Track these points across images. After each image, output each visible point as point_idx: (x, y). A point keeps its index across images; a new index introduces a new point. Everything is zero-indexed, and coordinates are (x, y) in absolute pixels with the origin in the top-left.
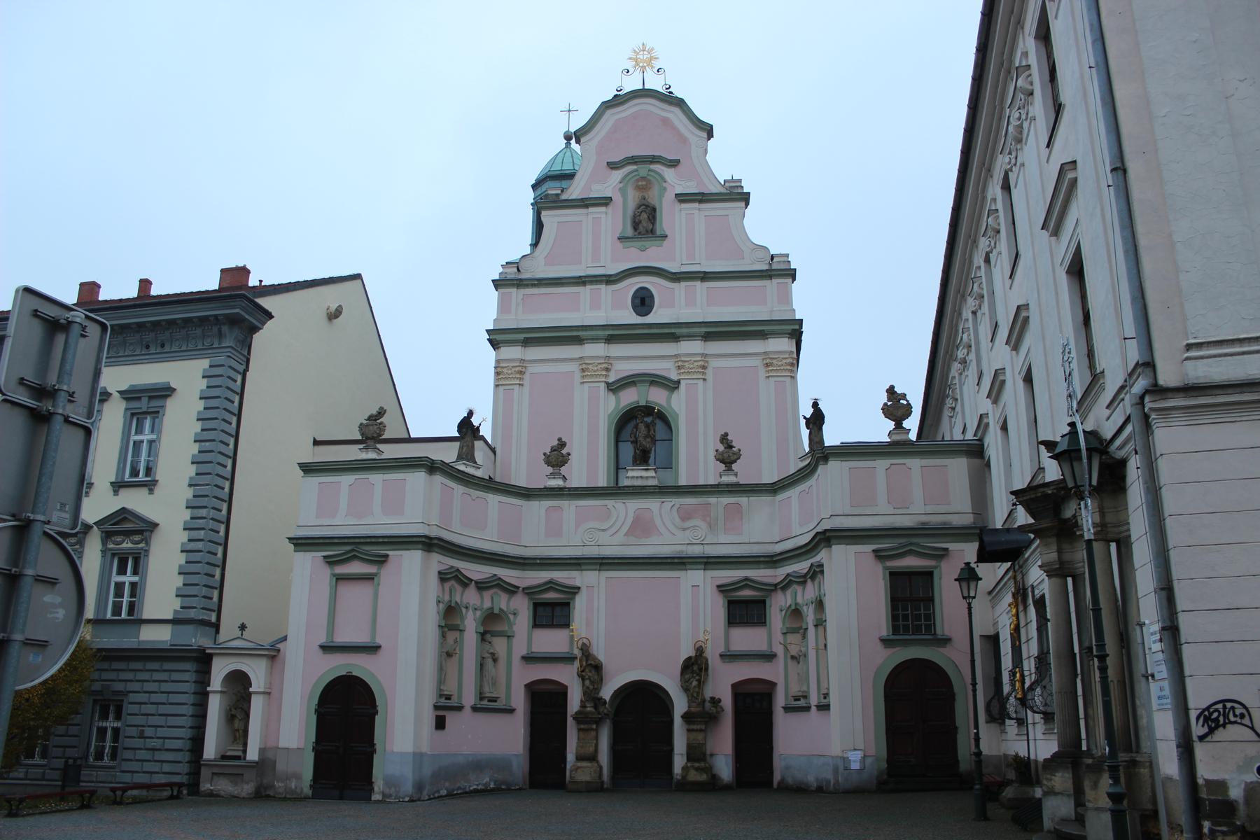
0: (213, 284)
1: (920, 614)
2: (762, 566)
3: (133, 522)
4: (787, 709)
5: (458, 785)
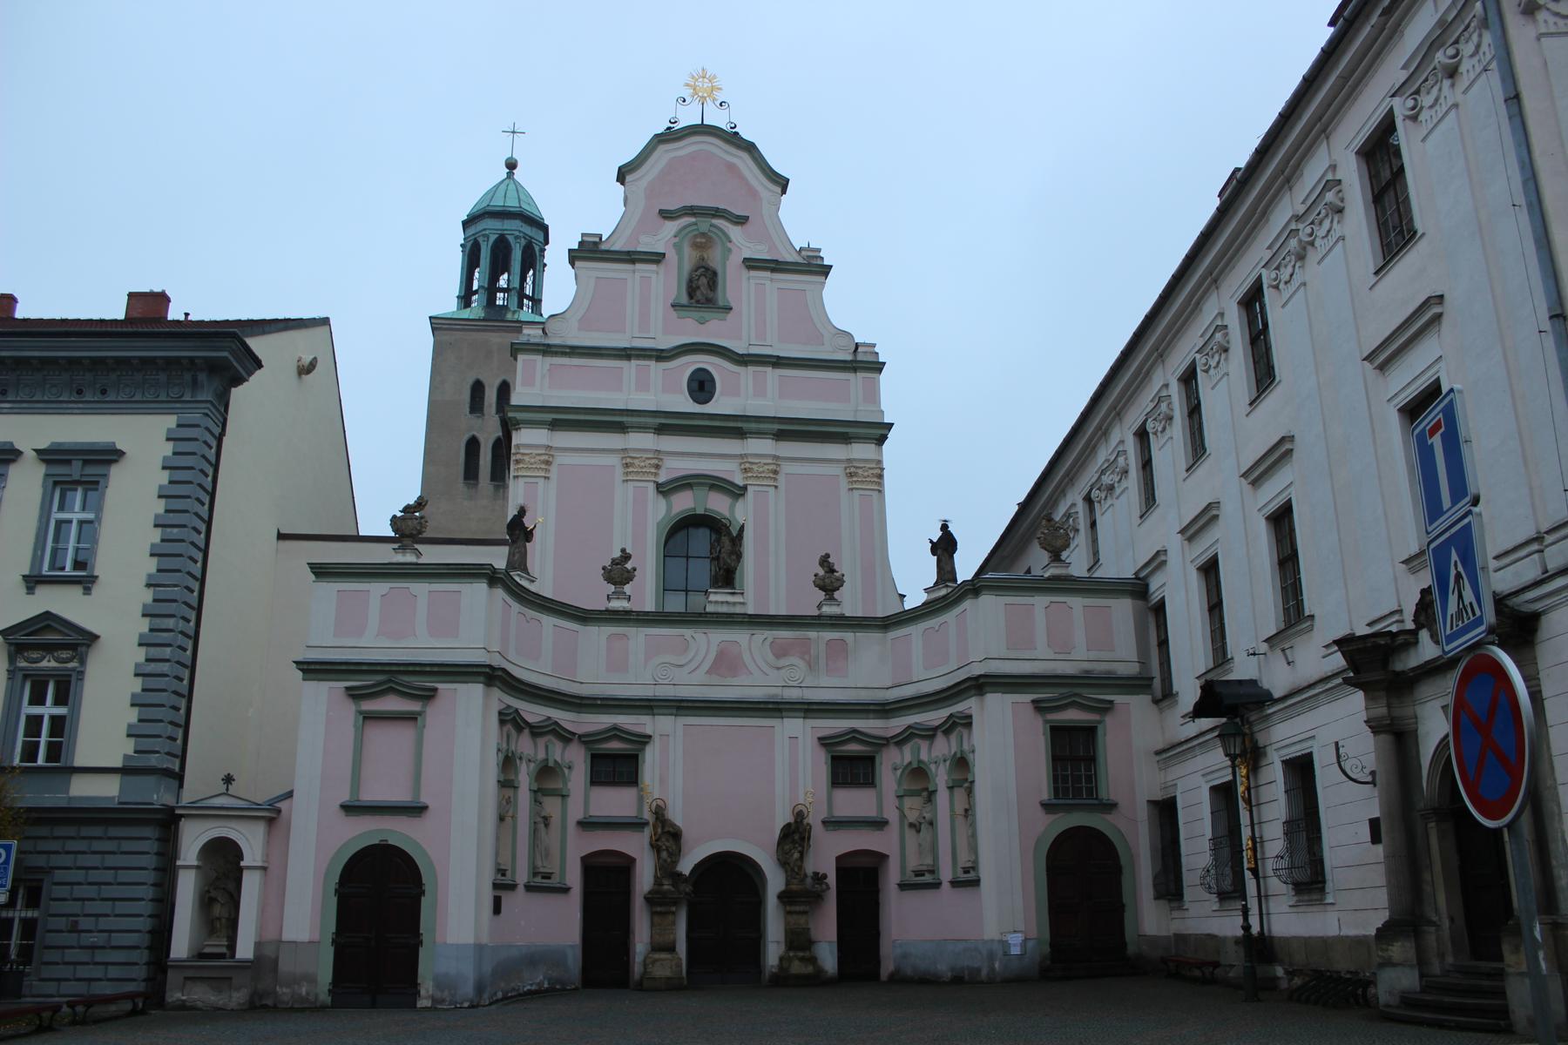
0: (116, 310)
1: (1081, 776)
2: (871, 715)
3: (60, 632)
4: (903, 886)
5: (513, 985)
